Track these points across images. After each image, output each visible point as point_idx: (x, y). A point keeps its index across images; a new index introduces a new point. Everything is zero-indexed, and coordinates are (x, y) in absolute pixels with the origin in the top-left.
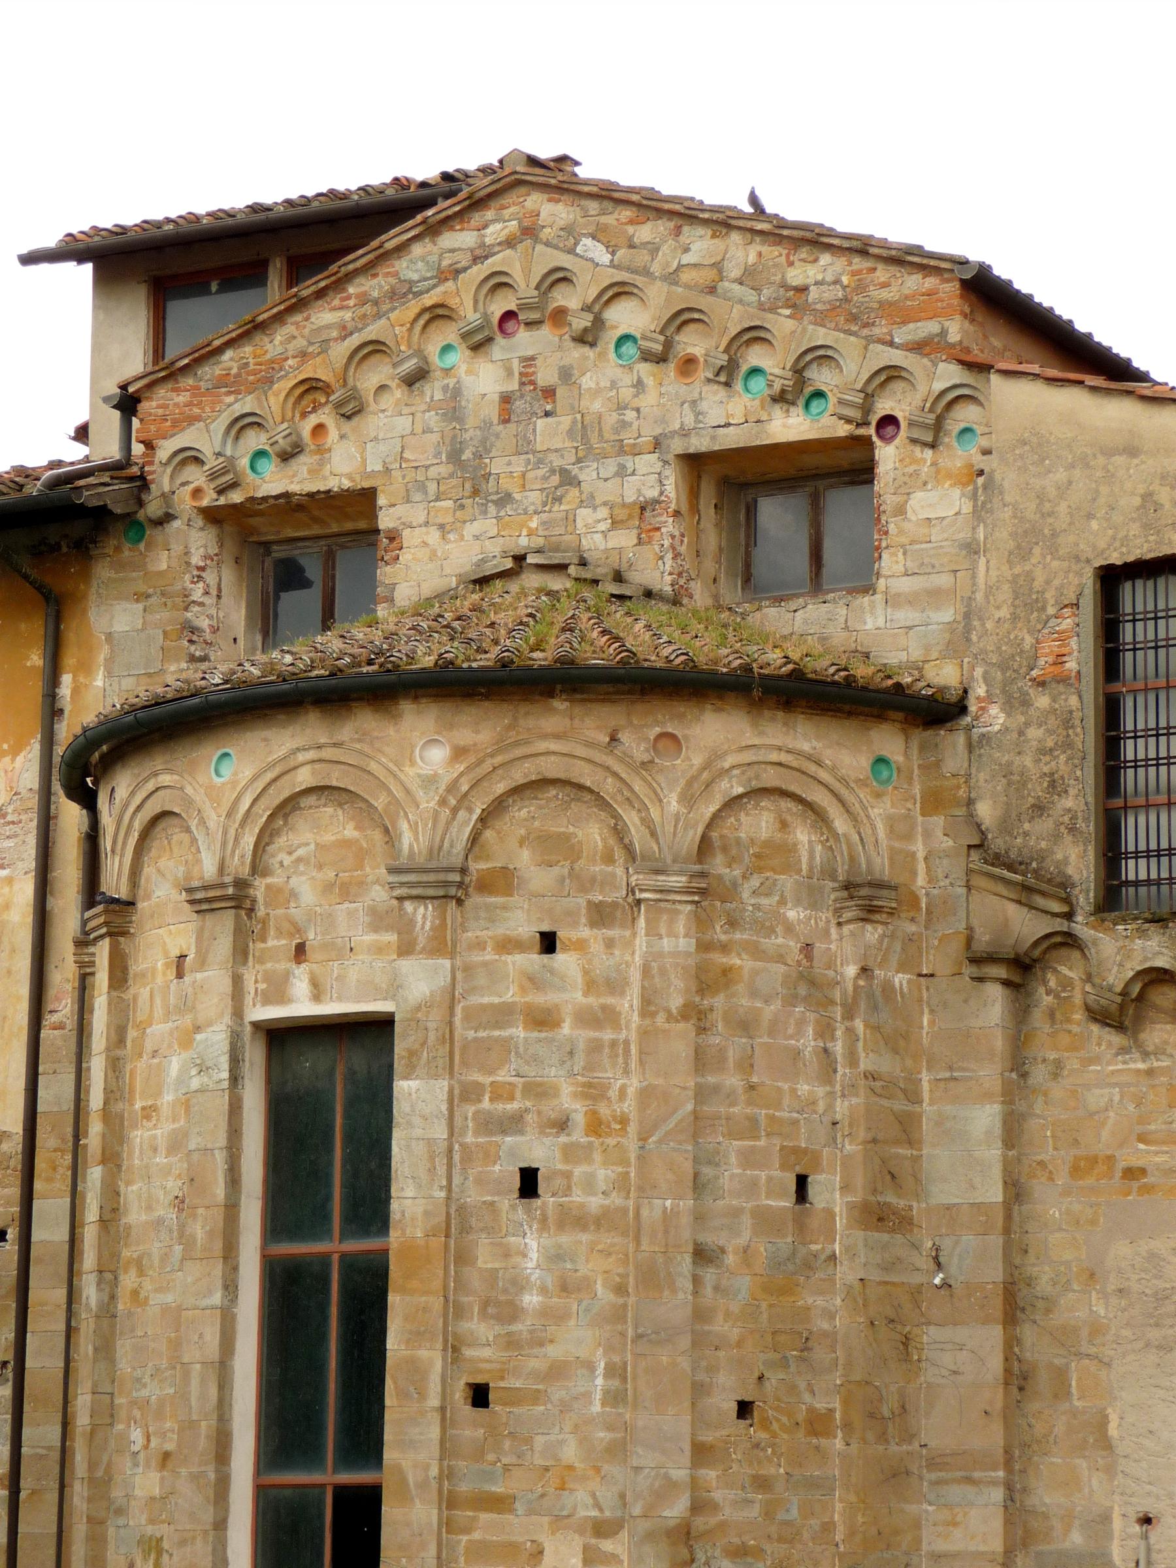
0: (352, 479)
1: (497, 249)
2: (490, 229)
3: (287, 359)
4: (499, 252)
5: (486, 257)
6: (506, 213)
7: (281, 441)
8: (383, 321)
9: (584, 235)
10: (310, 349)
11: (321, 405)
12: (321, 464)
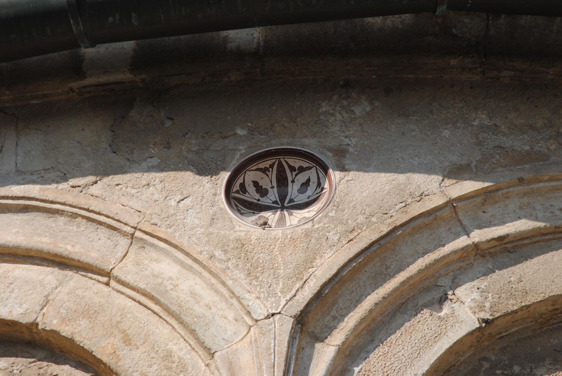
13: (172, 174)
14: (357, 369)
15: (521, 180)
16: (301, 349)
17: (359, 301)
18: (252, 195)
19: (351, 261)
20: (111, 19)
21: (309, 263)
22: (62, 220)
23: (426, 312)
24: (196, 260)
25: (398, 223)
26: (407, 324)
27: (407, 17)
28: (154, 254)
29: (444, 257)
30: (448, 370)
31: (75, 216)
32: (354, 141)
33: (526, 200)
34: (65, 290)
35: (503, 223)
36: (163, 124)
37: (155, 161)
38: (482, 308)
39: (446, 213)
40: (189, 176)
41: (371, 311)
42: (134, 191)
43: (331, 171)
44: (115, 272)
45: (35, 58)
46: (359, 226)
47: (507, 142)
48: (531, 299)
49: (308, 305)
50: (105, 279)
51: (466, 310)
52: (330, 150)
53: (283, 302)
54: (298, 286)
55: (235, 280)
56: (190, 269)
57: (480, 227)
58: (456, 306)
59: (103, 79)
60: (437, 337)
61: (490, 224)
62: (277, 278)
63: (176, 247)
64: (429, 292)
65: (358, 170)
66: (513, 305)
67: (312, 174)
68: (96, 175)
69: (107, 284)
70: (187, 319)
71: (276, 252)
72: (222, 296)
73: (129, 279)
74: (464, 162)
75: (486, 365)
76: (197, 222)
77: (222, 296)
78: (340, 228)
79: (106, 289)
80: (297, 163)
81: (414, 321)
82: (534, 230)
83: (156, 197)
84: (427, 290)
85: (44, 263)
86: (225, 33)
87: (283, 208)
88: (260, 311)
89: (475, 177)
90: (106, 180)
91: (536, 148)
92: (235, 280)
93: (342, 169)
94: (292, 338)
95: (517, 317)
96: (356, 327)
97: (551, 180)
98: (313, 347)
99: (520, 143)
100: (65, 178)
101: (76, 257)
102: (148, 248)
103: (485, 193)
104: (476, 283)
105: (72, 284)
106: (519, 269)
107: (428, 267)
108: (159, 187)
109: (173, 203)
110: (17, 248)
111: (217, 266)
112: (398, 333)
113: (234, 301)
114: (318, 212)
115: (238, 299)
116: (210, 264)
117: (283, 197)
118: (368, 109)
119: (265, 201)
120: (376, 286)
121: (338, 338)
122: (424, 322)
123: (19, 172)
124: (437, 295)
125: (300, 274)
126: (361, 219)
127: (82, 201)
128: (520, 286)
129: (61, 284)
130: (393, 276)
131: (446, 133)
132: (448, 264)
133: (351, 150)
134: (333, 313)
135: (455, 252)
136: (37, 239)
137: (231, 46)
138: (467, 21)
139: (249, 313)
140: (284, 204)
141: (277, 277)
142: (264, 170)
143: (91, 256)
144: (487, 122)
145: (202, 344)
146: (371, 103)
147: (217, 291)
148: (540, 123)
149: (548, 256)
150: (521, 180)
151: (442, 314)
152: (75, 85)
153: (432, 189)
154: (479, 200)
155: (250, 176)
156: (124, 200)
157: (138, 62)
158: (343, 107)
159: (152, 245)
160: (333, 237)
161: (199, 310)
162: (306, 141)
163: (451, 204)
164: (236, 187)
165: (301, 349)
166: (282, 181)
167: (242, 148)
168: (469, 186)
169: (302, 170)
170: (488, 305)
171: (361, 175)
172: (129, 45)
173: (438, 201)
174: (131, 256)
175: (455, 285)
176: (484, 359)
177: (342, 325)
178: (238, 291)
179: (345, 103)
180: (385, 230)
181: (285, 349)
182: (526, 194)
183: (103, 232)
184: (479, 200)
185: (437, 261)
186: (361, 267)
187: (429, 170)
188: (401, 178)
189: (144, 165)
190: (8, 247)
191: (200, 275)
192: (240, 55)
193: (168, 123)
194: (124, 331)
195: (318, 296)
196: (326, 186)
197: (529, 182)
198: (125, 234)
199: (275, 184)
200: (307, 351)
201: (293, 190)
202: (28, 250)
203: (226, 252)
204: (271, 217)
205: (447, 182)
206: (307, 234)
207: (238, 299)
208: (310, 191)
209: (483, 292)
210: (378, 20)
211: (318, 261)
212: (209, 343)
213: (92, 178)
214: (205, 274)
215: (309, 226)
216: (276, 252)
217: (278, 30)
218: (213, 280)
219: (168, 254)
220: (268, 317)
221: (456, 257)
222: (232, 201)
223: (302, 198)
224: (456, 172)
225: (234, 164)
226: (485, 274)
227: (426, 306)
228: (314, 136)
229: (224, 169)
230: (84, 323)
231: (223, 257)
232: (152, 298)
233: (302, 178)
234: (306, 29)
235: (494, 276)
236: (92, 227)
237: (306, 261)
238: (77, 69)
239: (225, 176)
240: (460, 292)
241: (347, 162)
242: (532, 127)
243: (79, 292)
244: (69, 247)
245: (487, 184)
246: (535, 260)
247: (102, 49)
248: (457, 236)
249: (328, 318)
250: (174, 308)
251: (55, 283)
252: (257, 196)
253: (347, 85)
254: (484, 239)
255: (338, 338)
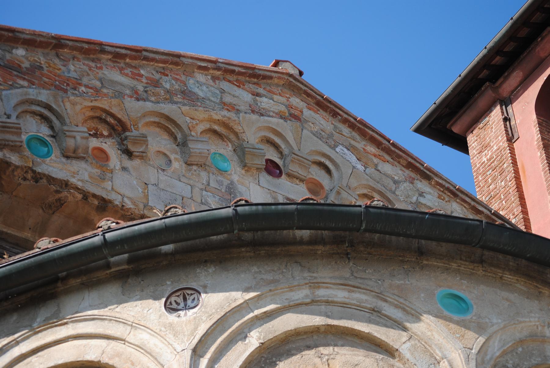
0: (134, 203)
1: (271, 114)
2: (264, 99)
3: (80, 84)
4: (272, 117)
5: (262, 115)
6: (276, 97)
7: (78, 138)
8: (174, 107)
9: (342, 144)
10: (105, 91)
11: (102, 135)
12: (103, 179)
13: (144, 301)
14: (216, 366)
15: (270, 290)
16: (195, 361)
17: (215, 341)
18: (174, 306)
19: (211, 327)
20: (117, 248)
21: (196, 329)
22: (106, 322)
23: (240, 342)
24: (155, 332)
25: (227, 311)
26: (234, 348)
27: (225, 235)
28: (140, 331)
29: (245, 322)
30: (250, 363)
31: (111, 320)
32: (210, 282)
33: (273, 297)
34: (110, 347)
35: (265, 306)
36: (140, 283)
37: (138, 297)
38: (260, 339)
39: (245, 305)
40: (151, 301)
41: (220, 344)
42: (131, 309)
43: (202, 294)
44: (127, 339)
45: (93, 264)
46: (213, 313)
47: (264, 277)
48: (277, 333)
49: (197, 345)
50: (123, 342)
51: (254, 340)
52: (201, 286)
53: (187, 345)
54: (192, 338)
55: (169, 338)
56: (153, 335)
57: (257, 309)
58: (250, 339)
59: (118, 269)
60: (245, 351)
61: (261, 308)
62: (184, 335)
63: (147, 328)
64: (241, 335)
65: (212, 292)
66: (271, 336)
67: (195, 296)
68: (117, 304)
69: (124, 344)
70: (154, 354)
71: (184, 326)
72: (165, 344)
73: (132, 341)
74: (250, 286)
75: (263, 359)
76: (154, 318)
77: (165, 344)
78: (206, 315)
79: (124, 346)
80: (190, 292)
81: (236, 346)
82: (276, 308)
83: (139, 310)
84: (240, 334)
85: (532, 46)
86: (160, 247)
87: (186, 309)
88: (179, 349)
89: (254, 291)
90: (121, 306)
91: (275, 278)
92: (169, 338)
93: (206, 293)
94: (191, 358)
95: (273, 340)
96: (215, 351)
97: (281, 289)
98: (199, 360)
99: (269, 277)
100: (106, 307)
101: (112, 335)
102: (138, 329)
103: (258, 296)
104: (257, 330)
105: (112, 345)
106: (272, 323)
107: (240, 326)
108: (140, 306)
109: (145, 312)
110: (91, 334)
111: (162, 334)
112: (230, 351)
113: (170, 346)
114: (199, 309)
115: (171, 345)
116: (160, 333)
117: (186, 305)
118: (214, 270)
119: (180, 307)
120: (221, 334)
121: (208, 355)
122: (240, 345)
123: (90, 306)
124: (243, 336)
125: (193, 333)
126: (214, 311)
127: (113, 314)
128: (273, 329)
129: (108, 345)
130: (227, 330)
131: (243, 276)
132: (247, 324)
133: (209, 285)
134: (206, 347)
135: (249, 319)
136: (98, 330)
137: (163, 252)
138: (246, 234)
139: (175, 350)
140: (186, 308)
141: (184, 335)
142: (178, 296)
143: (118, 334)
144: (257, 270)
145: (159, 363)
146: (215, 267)
147: (163, 343)
148: (276, 269)
149: (280, 318)
150: (270, 290)
151: (246, 342)
152: (108, 272)
153: (239, 297)
154: (256, 299)
155: (173, 299)
156: (128, 312)
157: (129, 261)
158: (205, 270)
159: (139, 328)
160: (204, 318)
161: (157, 350)
162: (192, 284)
163: (246, 302)
164: (168, 303)
165: (195, 361)
166: (185, 299)
167: (169, 289)
168: (252, 295)
169: (192, 294)
170: (262, 337)
171: (213, 294)
172: (126, 256)
173: (241, 301)
174: (132, 333)
175: (250, 331)
176: (263, 357)
177: (210, 351)
178: (171, 342)
179: (205, 268)
180: (223, 314)
181: (189, 362)
182: (272, 295)
183: (121, 325)
184: (256, 299)
185: (242, 323)
186: (213, 330)
187: (237, 290)
188: (227, 294)
189: (134, 298)
190: (88, 334)
191: (157, 337)
192: (166, 254)
193: (142, 282)
194: (131, 361)
195: (200, 341)
196: (201, 300)
197: (274, 291)
198: (129, 325)
199: (182, 300)
200: (197, 362)
201: (189, 302)
202: (95, 334)
203: (165, 328)
204: (182, 313)
205: (244, 294)
206: (195, 318)
207: (171, 345)
208: (195, 302)
209: (260, 333)
210: (215, 237)
211: (199, 328)
212: (162, 362)
213: (116, 306)
214: (159, 337)
215: (195, 315)
216: (184, 326)
217: (179, 245)
218: (162, 339)
219: (145, 331)
220: (182, 351)
221: (249, 321)
222: (167, 309)
223: (193, 305)
224: (247, 290)
225: (167, 295)
226: (260, 326)
227: (240, 340)
228: (195, 282)
229: (163, 297)
230: (117, 359)
231: (165, 330)
232: (140, 348)
233: (192, 297)
234: (189, 243)
235: (264, 326)
236: (118, 323)
237: (195, 328)
238: (108, 266)
239: (164, 300)
240: (252, 333)
241: (207, 290)
242: (273, 270)
243: (115, 348)
244: (110, 332)
245: (258, 293)
246: (278, 319)
247: (116, 258)
248: (249, 313)
249: (204, 348)
250: (148, 351)
251: (106, 345)
252: (176, 306)
253: (206, 261)
254: (259, 313)
255: (208, 355)
